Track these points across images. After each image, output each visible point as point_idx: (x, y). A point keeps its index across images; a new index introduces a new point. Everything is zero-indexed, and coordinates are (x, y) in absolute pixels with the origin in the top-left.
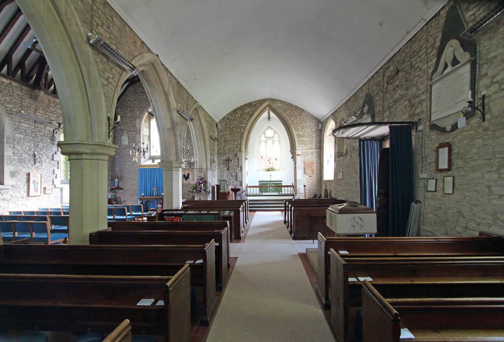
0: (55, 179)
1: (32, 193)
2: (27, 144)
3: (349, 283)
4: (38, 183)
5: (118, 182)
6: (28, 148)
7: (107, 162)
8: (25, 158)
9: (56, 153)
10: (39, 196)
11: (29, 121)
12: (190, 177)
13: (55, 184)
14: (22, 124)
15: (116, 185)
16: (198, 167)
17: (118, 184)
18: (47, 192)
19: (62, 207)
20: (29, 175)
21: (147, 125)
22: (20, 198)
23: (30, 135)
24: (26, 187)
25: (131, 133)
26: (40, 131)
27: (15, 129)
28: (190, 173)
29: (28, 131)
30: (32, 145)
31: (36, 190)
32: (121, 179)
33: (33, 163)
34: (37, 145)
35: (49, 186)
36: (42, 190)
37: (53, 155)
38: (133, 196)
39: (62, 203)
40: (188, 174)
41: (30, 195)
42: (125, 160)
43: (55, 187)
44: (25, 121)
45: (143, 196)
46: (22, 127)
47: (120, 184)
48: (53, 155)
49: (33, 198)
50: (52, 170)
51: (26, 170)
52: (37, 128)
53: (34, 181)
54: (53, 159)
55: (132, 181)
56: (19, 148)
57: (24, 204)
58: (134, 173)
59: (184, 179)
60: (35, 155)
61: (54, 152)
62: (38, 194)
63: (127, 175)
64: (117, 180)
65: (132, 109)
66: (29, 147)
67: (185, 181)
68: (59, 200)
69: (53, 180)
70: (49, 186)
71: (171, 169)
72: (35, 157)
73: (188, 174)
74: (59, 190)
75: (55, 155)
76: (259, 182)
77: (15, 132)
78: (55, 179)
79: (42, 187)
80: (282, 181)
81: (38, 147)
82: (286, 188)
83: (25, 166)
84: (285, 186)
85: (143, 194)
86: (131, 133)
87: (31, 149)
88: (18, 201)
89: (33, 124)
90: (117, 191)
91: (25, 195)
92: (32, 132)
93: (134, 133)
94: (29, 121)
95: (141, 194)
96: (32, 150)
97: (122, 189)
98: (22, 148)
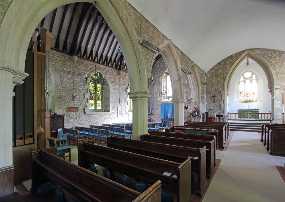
14: (115, 86)
15: (150, 112)
21: (165, 80)
24: (117, 113)
27: (113, 89)
31: (120, 115)
39: (129, 120)
40: (188, 106)
45: (163, 118)
47: (152, 112)
51: (117, 106)
53: (119, 110)
62: (121, 116)
65: (157, 73)
67: (185, 110)
73: (188, 106)
74: (128, 114)
76: (238, 110)
84: (262, 114)
85: (163, 117)
89: (119, 86)
90: (151, 115)
91: (117, 116)
97: (153, 114)
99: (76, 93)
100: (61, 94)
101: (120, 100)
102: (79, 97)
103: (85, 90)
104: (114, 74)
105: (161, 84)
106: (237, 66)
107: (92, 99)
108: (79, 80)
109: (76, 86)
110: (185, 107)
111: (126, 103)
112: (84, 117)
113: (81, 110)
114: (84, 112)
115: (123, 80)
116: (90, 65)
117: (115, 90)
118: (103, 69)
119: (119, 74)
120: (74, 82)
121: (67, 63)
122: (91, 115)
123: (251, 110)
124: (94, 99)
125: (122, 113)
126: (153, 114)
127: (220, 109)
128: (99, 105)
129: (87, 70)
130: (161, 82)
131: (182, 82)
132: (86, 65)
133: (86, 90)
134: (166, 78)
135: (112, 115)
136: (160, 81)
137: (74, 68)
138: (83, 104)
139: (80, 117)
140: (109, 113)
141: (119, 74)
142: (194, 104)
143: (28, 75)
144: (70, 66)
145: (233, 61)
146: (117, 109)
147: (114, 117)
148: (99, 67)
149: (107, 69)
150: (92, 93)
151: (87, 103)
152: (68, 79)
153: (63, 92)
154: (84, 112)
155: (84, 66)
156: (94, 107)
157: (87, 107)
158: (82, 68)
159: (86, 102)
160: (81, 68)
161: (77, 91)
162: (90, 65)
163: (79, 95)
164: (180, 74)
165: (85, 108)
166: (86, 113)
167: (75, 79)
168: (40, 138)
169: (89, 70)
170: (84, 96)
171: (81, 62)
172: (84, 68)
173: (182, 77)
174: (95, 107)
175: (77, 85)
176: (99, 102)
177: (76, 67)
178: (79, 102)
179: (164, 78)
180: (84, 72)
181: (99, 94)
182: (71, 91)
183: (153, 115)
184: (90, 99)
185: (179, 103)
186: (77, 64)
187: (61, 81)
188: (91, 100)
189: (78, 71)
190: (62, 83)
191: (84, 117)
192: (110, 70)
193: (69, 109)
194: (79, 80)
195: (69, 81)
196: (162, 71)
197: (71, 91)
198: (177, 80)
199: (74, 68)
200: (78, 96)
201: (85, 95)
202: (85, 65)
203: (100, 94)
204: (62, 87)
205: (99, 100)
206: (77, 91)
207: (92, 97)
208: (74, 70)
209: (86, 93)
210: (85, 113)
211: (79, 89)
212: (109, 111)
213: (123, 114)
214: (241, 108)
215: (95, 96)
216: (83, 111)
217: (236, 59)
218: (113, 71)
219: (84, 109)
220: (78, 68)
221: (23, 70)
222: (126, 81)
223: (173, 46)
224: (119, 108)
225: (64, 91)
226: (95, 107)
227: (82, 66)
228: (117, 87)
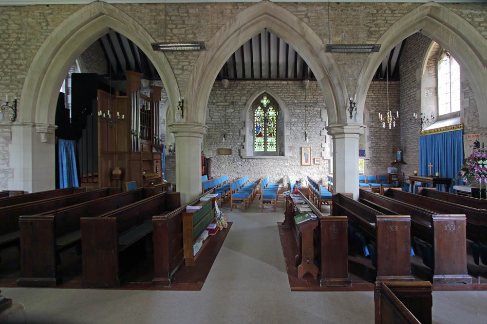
4: (308, 155)
14: (296, 111)
20: (301, 148)
22: (296, 167)
30: (304, 125)
31: (307, 161)
34: (308, 125)
43: (323, 158)
45: (416, 175)
53: (305, 153)
91: (299, 164)
93: (415, 90)
96: (304, 129)
97: (405, 164)
99: (228, 129)
100: (211, 133)
102: (233, 135)
103: (240, 123)
104: (293, 89)
107: (260, 135)
108: (232, 111)
109: (229, 120)
111: (322, 140)
112: (240, 163)
113: (236, 152)
114: (240, 155)
115: (313, 96)
116: (249, 86)
118: (270, 87)
119: (303, 87)
120: (226, 114)
121: (217, 92)
122: (250, 160)
124: (263, 135)
125: (312, 158)
126: (405, 164)
127: (322, 147)
128: (272, 145)
129: (244, 94)
131: (335, 81)
132: (242, 87)
133: (243, 124)
134: (324, 72)
135: (289, 161)
136: (418, 78)
137: (225, 97)
138: (238, 144)
139: (234, 162)
140: (282, 157)
141: (303, 87)
143: (57, 126)
144: (221, 94)
146: (299, 150)
148: (263, 85)
149: (278, 84)
150: (260, 127)
151: (244, 142)
152: (218, 112)
153: (213, 130)
154: (240, 155)
155: (240, 90)
156: (275, 148)
157: (243, 148)
158: (237, 93)
159: (242, 141)
160: (235, 94)
161: (229, 126)
162: (249, 86)
163: (232, 132)
164: (326, 62)
165: (242, 149)
166: (243, 157)
167: (227, 111)
169: (248, 93)
170: (240, 132)
171: (235, 85)
172: (239, 92)
173: (331, 68)
174: (265, 148)
175: (229, 118)
176: (272, 140)
177: (228, 93)
178: (233, 141)
180: (238, 98)
181: (272, 126)
182: (222, 128)
183: (406, 166)
184: (257, 136)
186: (229, 90)
187: (210, 116)
188: (259, 138)
189: (232, 98)
190: (211, 119)
191: (240, 163)
192: (284, 85)
193: (219, 152)
194: (232, 111)
195: (219, 114)
197: (222, 128)
198: (322, 79)
199: (225, 97)
200: (231, 133)
201: (241, 130)
202: (241, 88)
203: (274, 126)
204: (212, 124)
205: (271, 136)
206: (229, 126)
207: (261, 133)
208: (226, 98)
209: (242, 128)
210: (241, 157)
211: (233, 123)
212: (283, 154)
213: (314, 159)
215: (265, 131)
216: (238, 154)
218: (292, 84)
219: (239, 151)
220: (231, 94)
221: (54, 123)
223: (279, 8)
225: (214, 128)
226: (265, 148)
227: (236, 90)
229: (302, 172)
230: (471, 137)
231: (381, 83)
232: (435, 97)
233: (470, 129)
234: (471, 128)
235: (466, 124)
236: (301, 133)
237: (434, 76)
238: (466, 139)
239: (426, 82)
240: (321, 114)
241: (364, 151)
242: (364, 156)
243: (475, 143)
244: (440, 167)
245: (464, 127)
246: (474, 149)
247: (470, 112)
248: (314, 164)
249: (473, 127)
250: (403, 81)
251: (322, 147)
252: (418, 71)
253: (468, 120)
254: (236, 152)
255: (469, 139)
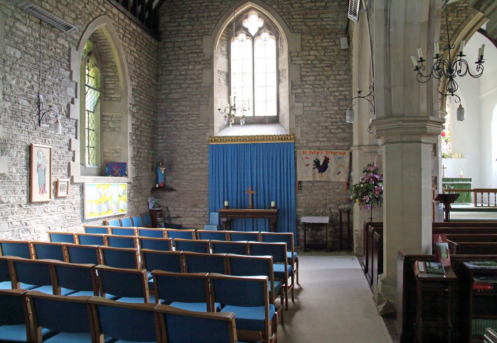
0: (72, 162)
1: (36, 197)
2: (26, 73)
3: (58, 289)
4: (45, 171)
5: (165, 175)
6: (28, 84)
7: (252, 115)
8: (23, 109)
9: (73, 102)
10: (47, 202)
11: (31, 20)
12: (331, 165)
13: (71, 175)
14: (18, 25)
15: (161, 180)
16: (366, 142)
17: (165, 179)
18: (60, 194)
19: (86, 229)
20: (30, 149)
21: (224, 49)
22: (16, 208)
23: (32, 52)
24: (25, 180)
25: (191, 67)
26: (49, 46)
27: (6, 36)
28: (331, 156)
29: (29, 44)
30: (36, 77)
31: (42, 191)
32: (170, 167)
33: (36, 122)
34: (44, 80)
35: (64, 181)
36: (53, 187)
37: (68, 107)
38: (196, 206)
39: (83, 220)
40: (327, 160)
41: (34, 199)
42: (178, 126)
43: (72, 180)
44: (23, 17)
45: (228, 207)
46: (19, 33)
47: (168, 178)
48: (68, 107)
49: (37, 207)
50: (67, 142)
51: (24, 139)
52: (44, 37)
53: (39, 166)
54: (68, 116)
55: (192, 173)
56: (14, 82)
57: (24, 221)
58: (198, 154)
59: (316, 170)
60: (39, 103)
61: (70, 100)
62: (45, 197)
63: (183, 158)
64: (162, 170)
65: (193, 16)
66: (30, 82)
67: (318, 175)
68: (79, 211)
69: (69, 164)
70: (64, 181)
71: (416, 138)
72: (39, 106)
73: (327, 160)
74: (77, 189)
75: (71, 105)
76: (39, 194)
77: (6, 40)
78: (72, 162)
79: (52, 181)
80: (470, 180)
81: (46, 82)
82: (485, 194)
83: (23, 127)
84: (476, 191)
85: (226, 203)
86: (191, 67)
87: (33, 87)
88: (13, 213)
89: (36, 27)
90: (161, 193)
91: (24, 199)
92: (36, 47)
93: (198, 67)
94: (31, 20)
95: (270, 204)
96: (36, 89)
97: (172, 190)
98: (18, 83)
101: (44, 107)
105: (209, 63)
106: (469, 36)
110: (317, 162)
117: (16, 46)
123: (452, 180)
127: (70, 149)
130: (212, 56)
142: (366, 150)
145: (458, 21)
147: (12, 200)
168: (164, 27)
179: (221, 40)
185: (423, 140)
196: (214, 11)
214: (462, 173)
217: (467, 17)
222: (73, 15)
224: (35, 150)
228: (25, 29)
229: (32, 224)
230: (308, 153)
231: (145, 35)
232: (225, 87)
233: (303, 144)
234: (305, 142)
235: (298, 136)
236: (30, 102)
237: (226, 56)
238: (301, 155)
239: (220, 63)
240: (69, 61)
241: (125, 164)
242: (126, 175)
243: (315, 161)
244: (226, 192)
245: (295, 139)
246: (314, 168)
247: (304, 122)
248: (56, 196)
249: (307, 141)
250: (168, 45)
251: (70, 149)
252: (207, 39)
253: (301, 132)
254: (67, 139)
255: (304, 156)
